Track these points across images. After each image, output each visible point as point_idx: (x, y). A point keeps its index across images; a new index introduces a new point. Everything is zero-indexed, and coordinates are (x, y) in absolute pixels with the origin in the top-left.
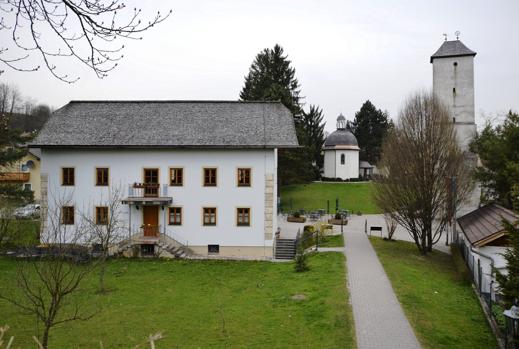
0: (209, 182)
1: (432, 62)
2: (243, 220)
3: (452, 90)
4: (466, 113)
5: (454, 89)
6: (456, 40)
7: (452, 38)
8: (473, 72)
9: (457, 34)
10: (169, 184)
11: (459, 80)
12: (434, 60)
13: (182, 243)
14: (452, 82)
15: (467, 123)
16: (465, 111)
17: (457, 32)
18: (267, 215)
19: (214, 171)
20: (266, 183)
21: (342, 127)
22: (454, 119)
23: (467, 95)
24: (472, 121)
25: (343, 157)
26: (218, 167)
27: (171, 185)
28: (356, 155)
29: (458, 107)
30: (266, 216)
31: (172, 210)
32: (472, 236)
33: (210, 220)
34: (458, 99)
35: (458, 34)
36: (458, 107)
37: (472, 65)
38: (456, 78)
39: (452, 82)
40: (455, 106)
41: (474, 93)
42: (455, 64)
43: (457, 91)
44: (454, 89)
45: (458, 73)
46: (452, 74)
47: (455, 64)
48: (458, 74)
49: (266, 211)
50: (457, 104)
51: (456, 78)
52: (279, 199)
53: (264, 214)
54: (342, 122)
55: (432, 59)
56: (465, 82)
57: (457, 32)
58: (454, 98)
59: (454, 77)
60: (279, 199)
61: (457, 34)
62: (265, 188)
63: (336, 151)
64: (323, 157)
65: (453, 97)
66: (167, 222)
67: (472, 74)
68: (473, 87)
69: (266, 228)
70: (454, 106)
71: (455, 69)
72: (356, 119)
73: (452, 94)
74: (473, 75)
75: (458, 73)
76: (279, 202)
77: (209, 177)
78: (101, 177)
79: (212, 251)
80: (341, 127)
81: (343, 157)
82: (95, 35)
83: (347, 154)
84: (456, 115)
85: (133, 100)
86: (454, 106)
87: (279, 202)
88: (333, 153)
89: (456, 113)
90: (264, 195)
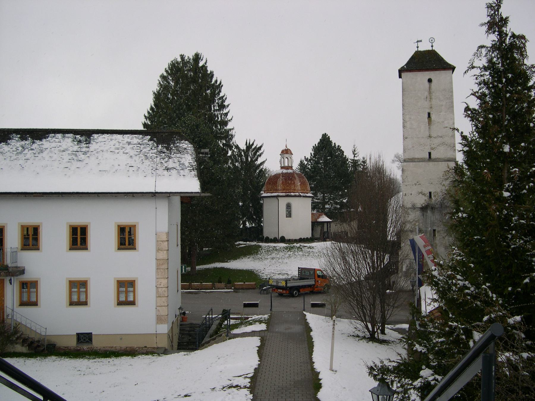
0: (77, 244)
1: (400, 77)
2: (126, 297)
3: (427, 116)
4: (445, 146)
5: (429, 114)
6: (430, 49)
7: (425, 47)
8: (452, 92)
9: (432, 41)
10: (20, 247)
11: (434, 102)
12: (403, 74)
13: (38, 331)
14: (426, 104)
15: (446, 159)
16: (443, 144)
17: (431, 39)
18: (160, 290)
19: (36, 230)
20: (157, 245)
21: (288, 165)
22: (430, 154)
23: (446, 122)
24: (452, 157)
25: (289, 206)
26: (138, 223)
27: (23, 249)
28: (308, 203)
29: (435, 138)
30: (157, 292)
31: (24, 285)
32: (435, 312)
33: (79, 297)
34: (433, 127)
35: (433, 41)
36: (435, 138)
37: (451, 83)
38: (431, 98)
39: (426, 104)
40: (430, 137)
41: (454, 120)
42: (430, 81)
43: (433, 117)
44: (429, 114)
45: (433, 92)
46: (426, 94)
47: (430, 81)
48: (433, 94)
49: (157, 283)
50: (434, 134)
51: (431, 98)
52: (183, 267)
53: (155, 288)
54: (287, 158)
55: (401, 71)
56: (442, 106)
57: (431, 39)
58: (429, 125)
59: (428, 97)
60: (183, 267)
61: (432, 41)
62: (156, 253)
63: (279, 198)
64: (262, 206)
65: (428, 124)
66: (17, 302)
67: (450, 94)
68: (452, 112)
69: (158, 308)
70: (429, 137)
71: (430, 88)
72: (313, 154)
73: (427, 120)
74: (452, 96)
75: (433, 92)
76: (183, 272)
77: (77, 237)
78: (81, 235)
79: (82, 342)
80: (286, 165)
81: (289, 206)
82: (491, 41)
83: (295, 203)
84: (432, 149)
85: (99, 128)
86: (429, 137)
87: (183, 272)
88: (275, 200)
89: (432, 146)
90: (154, 262)
